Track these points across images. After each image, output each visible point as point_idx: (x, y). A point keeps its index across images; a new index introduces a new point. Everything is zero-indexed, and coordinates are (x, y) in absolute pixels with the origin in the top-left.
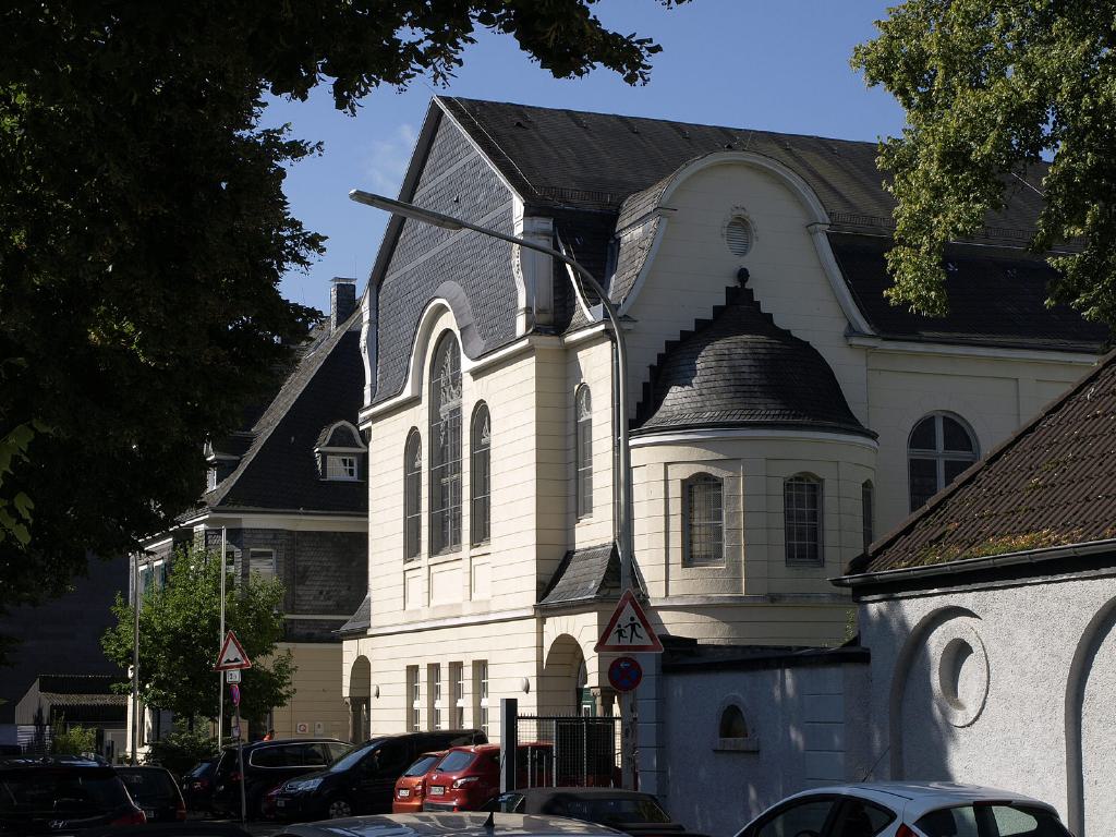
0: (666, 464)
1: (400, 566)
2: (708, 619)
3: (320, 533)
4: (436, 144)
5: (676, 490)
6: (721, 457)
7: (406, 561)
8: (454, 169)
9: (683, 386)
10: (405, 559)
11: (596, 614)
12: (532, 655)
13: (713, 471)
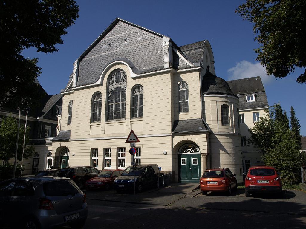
0: (90, 126)
1: (89, 124)
2: (228, 138)
3: (54, 120)
4: (109, 33)
5: (219, 108)
6: (229, 101)
7: (91, 123)
8: (120, 35)
9: (214, 85)
10: (90, 122)
11: (206, 135)
12: (171, 148)
13: (227, 104)
